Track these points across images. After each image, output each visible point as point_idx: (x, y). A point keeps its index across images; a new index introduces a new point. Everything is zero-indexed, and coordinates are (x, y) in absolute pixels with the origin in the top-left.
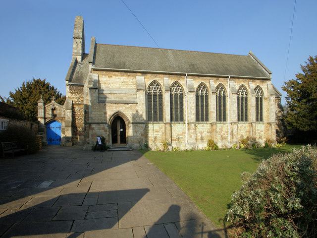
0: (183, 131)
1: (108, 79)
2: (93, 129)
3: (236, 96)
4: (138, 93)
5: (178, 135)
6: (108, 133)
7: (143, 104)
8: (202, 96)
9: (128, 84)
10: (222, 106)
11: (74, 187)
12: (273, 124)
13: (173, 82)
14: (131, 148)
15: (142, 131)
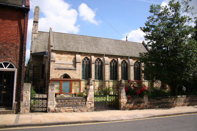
8: (124, 67)
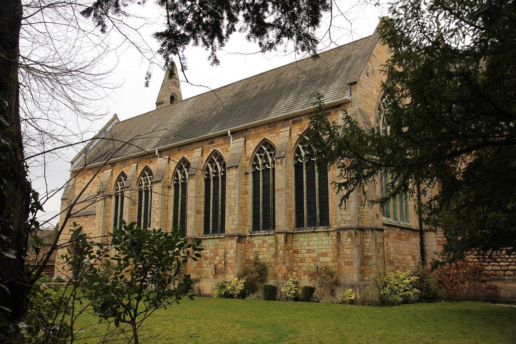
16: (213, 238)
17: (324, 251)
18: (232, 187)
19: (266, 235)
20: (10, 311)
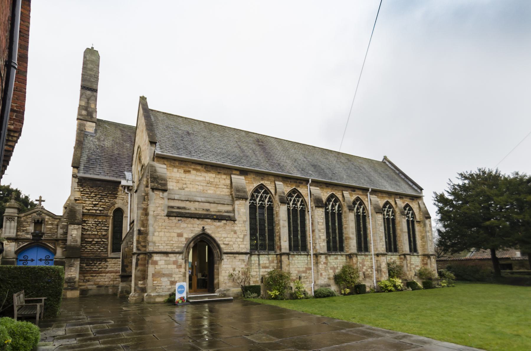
0: (306, 266)
1: (183, 175)
2: (155, 263)
3: (380, 217)
4: (237, 202)
5: (299, 272)
6: (183, 270)
7: (244, 222)
9: (216, 186)
10: (362, 229)
11: (72, 334)
12: (432, 257)
13: (255, 185)
14: (225, 296)
15: (243, 266)
16: (362, 255)
17: (417, 264)
18: (380, 225)
19: (392, 255)
20: (207, 246)
